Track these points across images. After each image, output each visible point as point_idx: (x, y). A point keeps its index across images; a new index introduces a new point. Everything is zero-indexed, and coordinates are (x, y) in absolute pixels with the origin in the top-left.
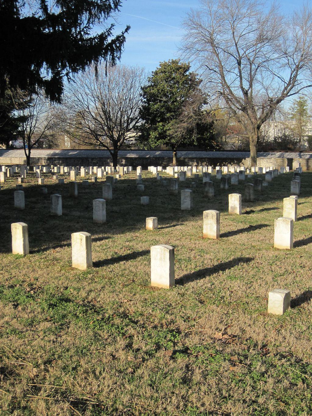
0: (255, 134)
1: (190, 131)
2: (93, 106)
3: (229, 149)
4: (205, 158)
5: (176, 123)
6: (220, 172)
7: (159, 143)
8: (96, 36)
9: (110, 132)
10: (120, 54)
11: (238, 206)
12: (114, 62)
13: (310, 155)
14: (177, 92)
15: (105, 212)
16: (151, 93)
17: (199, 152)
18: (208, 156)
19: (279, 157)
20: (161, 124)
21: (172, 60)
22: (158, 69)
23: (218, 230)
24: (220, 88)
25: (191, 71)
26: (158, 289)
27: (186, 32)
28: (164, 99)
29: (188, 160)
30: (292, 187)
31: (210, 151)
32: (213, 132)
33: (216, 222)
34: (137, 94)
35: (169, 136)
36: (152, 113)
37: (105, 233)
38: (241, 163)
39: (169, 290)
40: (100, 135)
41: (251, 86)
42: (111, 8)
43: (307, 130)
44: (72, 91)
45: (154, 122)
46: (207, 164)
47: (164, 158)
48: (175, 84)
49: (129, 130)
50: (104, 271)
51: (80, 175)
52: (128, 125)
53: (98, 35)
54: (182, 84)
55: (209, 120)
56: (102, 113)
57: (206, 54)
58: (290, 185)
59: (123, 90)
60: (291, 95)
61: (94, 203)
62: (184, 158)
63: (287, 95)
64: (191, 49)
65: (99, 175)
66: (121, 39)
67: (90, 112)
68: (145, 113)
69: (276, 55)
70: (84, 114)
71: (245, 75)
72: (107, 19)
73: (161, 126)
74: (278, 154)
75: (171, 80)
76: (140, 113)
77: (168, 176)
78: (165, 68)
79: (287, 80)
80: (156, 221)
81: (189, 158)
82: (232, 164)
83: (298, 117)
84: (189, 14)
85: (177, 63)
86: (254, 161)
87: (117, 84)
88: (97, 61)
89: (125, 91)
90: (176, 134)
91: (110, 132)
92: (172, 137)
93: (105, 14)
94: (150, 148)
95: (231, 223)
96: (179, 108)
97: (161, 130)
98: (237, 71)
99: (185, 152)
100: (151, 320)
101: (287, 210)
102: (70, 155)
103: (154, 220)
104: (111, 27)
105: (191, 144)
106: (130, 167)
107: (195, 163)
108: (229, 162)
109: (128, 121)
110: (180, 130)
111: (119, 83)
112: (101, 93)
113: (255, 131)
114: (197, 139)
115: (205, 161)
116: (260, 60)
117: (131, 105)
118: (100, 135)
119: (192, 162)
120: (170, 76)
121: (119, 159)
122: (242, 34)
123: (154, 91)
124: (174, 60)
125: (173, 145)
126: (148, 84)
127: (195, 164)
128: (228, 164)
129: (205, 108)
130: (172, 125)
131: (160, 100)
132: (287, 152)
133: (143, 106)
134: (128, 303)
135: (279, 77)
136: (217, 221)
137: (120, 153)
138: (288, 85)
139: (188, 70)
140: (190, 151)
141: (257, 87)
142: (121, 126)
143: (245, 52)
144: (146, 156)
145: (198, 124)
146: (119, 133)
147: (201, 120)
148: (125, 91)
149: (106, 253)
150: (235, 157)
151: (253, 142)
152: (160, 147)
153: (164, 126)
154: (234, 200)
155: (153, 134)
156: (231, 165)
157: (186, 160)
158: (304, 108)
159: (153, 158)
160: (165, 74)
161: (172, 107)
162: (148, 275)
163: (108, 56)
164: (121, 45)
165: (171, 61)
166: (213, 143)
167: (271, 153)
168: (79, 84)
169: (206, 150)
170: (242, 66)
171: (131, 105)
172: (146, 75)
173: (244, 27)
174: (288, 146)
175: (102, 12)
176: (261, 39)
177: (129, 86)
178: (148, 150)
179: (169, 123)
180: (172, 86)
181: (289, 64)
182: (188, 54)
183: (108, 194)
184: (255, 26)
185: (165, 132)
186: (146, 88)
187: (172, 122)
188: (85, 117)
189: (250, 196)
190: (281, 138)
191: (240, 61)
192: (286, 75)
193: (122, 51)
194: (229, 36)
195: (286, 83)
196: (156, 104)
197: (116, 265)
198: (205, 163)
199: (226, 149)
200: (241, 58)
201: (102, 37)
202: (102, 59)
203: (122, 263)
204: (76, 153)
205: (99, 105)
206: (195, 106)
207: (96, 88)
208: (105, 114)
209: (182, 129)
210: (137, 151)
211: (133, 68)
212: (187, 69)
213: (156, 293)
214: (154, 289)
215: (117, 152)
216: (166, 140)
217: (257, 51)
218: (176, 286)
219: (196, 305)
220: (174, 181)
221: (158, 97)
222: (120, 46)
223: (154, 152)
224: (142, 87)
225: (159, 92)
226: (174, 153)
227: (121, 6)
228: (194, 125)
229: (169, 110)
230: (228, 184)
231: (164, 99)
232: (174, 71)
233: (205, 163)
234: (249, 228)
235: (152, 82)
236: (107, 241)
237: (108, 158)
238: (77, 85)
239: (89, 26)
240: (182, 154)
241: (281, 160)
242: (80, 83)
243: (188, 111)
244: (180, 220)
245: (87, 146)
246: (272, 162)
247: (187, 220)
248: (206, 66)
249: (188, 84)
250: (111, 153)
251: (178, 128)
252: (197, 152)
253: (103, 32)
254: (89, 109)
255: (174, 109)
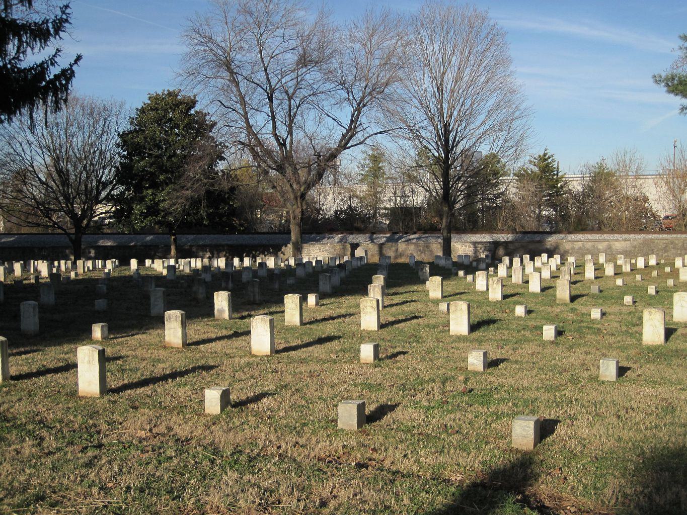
0: (298, 207)
1: (195, 203)
2: (41, 161)
3: (264, 230)
4: (223, 246)
5: (174, 190)
6: (263, 265)
7: (148, 221)
8: (33, 66)
9: (69, 204)
10: (67, 96)
11: (226, 308)
12: (57, 106)
13: (386, 237)
14: (176, 142)
15: (37, 320)
16: (134, 143)
17: (216, 236)
18: (229, 243)
19: (338, 242)
20: (150, 192)
21: (168, 90)
22: (145, 104)
23: (184, 335)
24: (243, 137)
25: (198, 108)
26: (86, 398)
27: (186, 49)
28: (156, 152)
29: (197, 249)
30: (321, 283)
31: (231, 234)
32: (233, 204)
33: (180, 325)
34: (112, 145)
35: (163, 211)
36: (136, 175)
37: (35, 345)
38: (280, 253)
39: (99, 398)
40: (55, 211)
41: (290, 132)
42: (50, 34)
43: (385, 199)
44: (5, 138)
45: (138, 188)
46: (227, 255)
47: (158, 246)
48: (172, 128)
49: (100, 202)
50: (21, 384)
51: (14, 274)
52: (99, 193)
53: (36, 64)
54: (183, 129)
55: (226, 186)
56: (55, 175)
57: (220, 82)
58: (318, 280)
59: (89, 136)
60: (352, 146)
61: (22, 307)
62: (191, 246)
63: (345, 147)
64: (196, 74)
65: (45, 273)
66: (69, 74)
67: (35, 172)
68: (125, 174)
69: (328, 86)
70: (24, 176)
71: (280, 116)
72: (43, 49)
73: (151, 195)
74: (338, 237)
75: (166, 122)
76: (116, 175)
77: (154, 273)
78: (156, 103)
79: (346, 122)
80: (106, 329)
81: (198, 246)
83: (370, 179)
84: (193, 20)
85: (177, 95)
86: (298, 249)
87: (81, 128)
88: (33, 105)
89: (93, 138)
90: (174, 208)
91: (69, 204)
92: (168, 214)
93: (41, 42)
94: (134, 231)
95: (212, 329)
96: (179, 167)
97: (151, 201)
98: (267, 109)
99: (192, 237)
100: (71, 426)
101: (289, 310)
102: (4, 242)
103: (102, 327)
104: (56, 53)
105: (199, 223)
106: (100, 261)
107: (209, 253)
108: (261, 250)
109: (98, 187)
110: (180, 201)
111: (84, 125)
112: (53, 142)
113: (297, 202)
114: (209, 215)
115: (224, 251)
116: (305, 92)
117: (102, 160)
118: (55, 211)
119: (203, 251)
120: (165, 116)
121: (84, 249)
122: (274, 54)
123: (139, 139)
124: (171, 89)
125: (170, 226)
126: (130, 128)
127: (208, 254)
129: (221, 166)
130: (169, 193)
131: (148, 154)
132: (352, 234)
133: (121, 163)
134: (46, 412)
135: (334, 119)
136: (182, 324)
137: (85, 239)
138: (348, 131)
139: (194, 107)
140: (201, 234)
141: (298, 135)
142: (86, 195)
143: (280, 80)
144: (130, 242)
145: (208, 192)
146: (84, 207)
147: (212, 185)
148: (93, 138)
149: (31, 366)
150: (271, 242)
151: (295, 218)
152: (153, 228)
153: (156, 195)
154: (221, 301)
155: (137, 209)
157: (194, 249)
158: (380, 165)
159: (141, 246)
160: (157, 113)
161: (168, 164)
162: (77, 384)
163: (50, 98)
164: (69, 83)
165: (166, 93)
166: (235, 221)
167: (327, 236)
168: (16, 127)
169: (224, 233)
170: (276, 102)
171: (102, 160)
172: (127, 113)
173: (277, 44)
174: (356, 225)
175: (37, 39)
176: (304, 61)
177: (99, 131)
178: (129, 234)
179: (163, 190)
180: (167, 131)
181: (349, 99)
182: (192, 83)
183: (49, 298)
184: (294, 42)
185: (157, 204)
186: (127, 135)
187: (167, 189)
188: (26, 180)
189: (254, 296)
190: (345, 211)
191: (272, 95)
192: (345, 115)
193: (69, 91)
194: (254, 55)
195: (345, 128)
196: (143, 158)
197: (41, 378)
198: (224, 253)
199: (259, 231)
200: (273, 90)
201: (42, 68)
202: (39, 102)
203: (49, 375)
204: (13, 239)
205: (48, 160)
206: (205, 164)
207: (45, 134)
208: (60, 176)
209: (183, 200)
210: (116, 236)
211: (105, 103)
212: (193, 103)
213: (83, 402)
214: (81, 398)
215: (81, 238)
216: (159, 218)
217: (299, 79)
218: (108, 394)
219: (126, 410)
221: (145, 148)
222: (67, 83)
223: (143, 236)
224: (119, 134)
225: (146, 141)
226: (173, 237)
227: (64, 31)
228: (202, 193)
229: (163, 169)
230: (232, 281)
231: (156, 152)
232: (171, 108)
233: (224, 253)
234: (233, 334)
235: (136, 125)
236: (35, 354)
237: (67, 248)
238: (14, 128)
239: (19, 56)
240: (187, 239)
241: (341, 247)
242: (18, 124)
243: (193, 171)
244: (144, 328)
245: (32, 228)
246: (327, 250)
247: (153, 328)
248: (220, 101)
249: (194, 128)
250: (71, 239)
251: (177, 198)
252: (212, 236)
253: (44, 60)
254: (33, 167)
255: (171, 168)
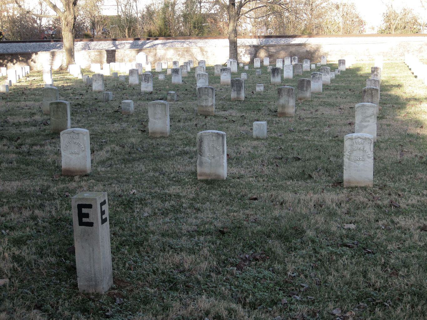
82: (15, 61)
113: (69, 9)
128: (7, 62)
156: (14, 64)
220: (210, 90)
